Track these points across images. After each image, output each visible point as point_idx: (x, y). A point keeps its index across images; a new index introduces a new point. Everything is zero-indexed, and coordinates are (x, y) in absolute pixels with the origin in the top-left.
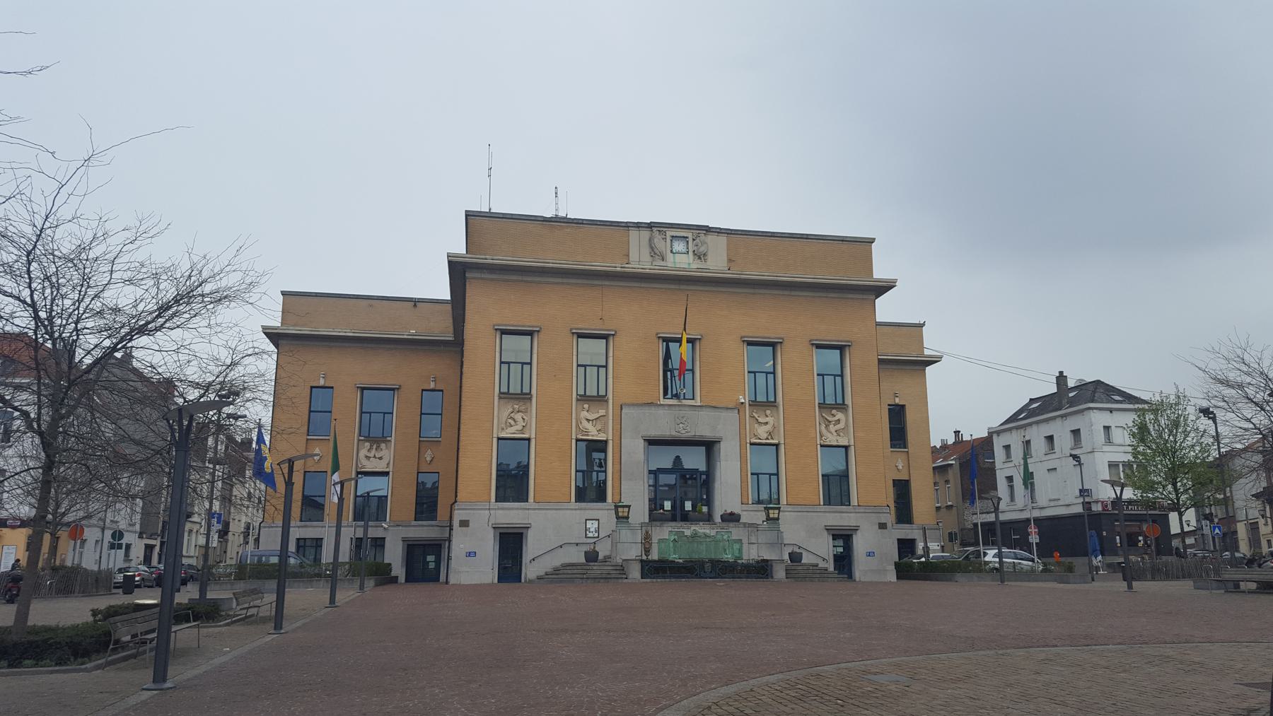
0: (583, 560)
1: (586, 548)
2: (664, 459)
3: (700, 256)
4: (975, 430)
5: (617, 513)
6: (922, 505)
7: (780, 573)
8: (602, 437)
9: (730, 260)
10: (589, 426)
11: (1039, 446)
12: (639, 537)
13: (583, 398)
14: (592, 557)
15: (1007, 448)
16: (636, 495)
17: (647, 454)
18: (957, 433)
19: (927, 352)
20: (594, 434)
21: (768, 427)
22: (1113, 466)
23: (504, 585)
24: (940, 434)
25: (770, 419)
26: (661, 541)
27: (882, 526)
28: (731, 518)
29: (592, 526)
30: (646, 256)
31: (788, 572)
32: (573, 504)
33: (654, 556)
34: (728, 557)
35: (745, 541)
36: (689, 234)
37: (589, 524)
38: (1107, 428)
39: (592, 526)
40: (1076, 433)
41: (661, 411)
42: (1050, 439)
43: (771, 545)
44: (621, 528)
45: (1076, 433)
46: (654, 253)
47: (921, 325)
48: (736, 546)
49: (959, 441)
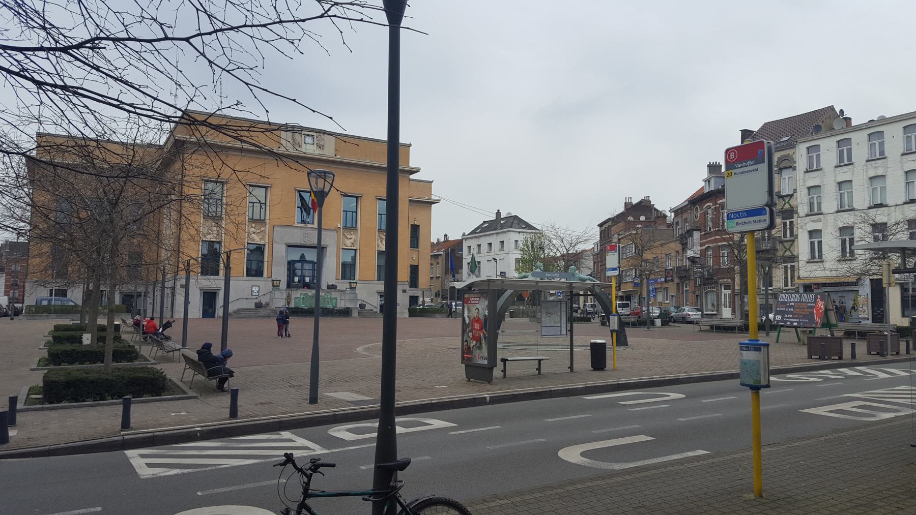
0: (253, 307)
1: (257, 301)
2: (295, 255)
3: (320, 147)
4: (454, 236)
5: (273, 284)
6: (423, 278)
7: (355, 314)
8: (262, 242)
9: (336, 150)
11: (484, 247)
12: (284, 296)
13: (252, 220)
14: (259, 305)
16: (280, 273)
17: (287, 252)
18: (446, 236)
19: (433, 197)
20: (257, 239)
21: (352, 241)
22: (517, 261)
24: (436, 235)
25: (353, 237)
28: (332, 287)
29: (256, 289)
31: (359, 313)
32: (245, 278)
33: (292, 305)
34: (330, 306)
36: (315, 134)
38: (516, 241)
39: (256, 289)
40: (502, 242)
41: (296, 230)
42: (490, 244)
43: (351, 300)
45: (502, 242)
46: (295, 144)
47: (431, 182)
49: (446, 240)
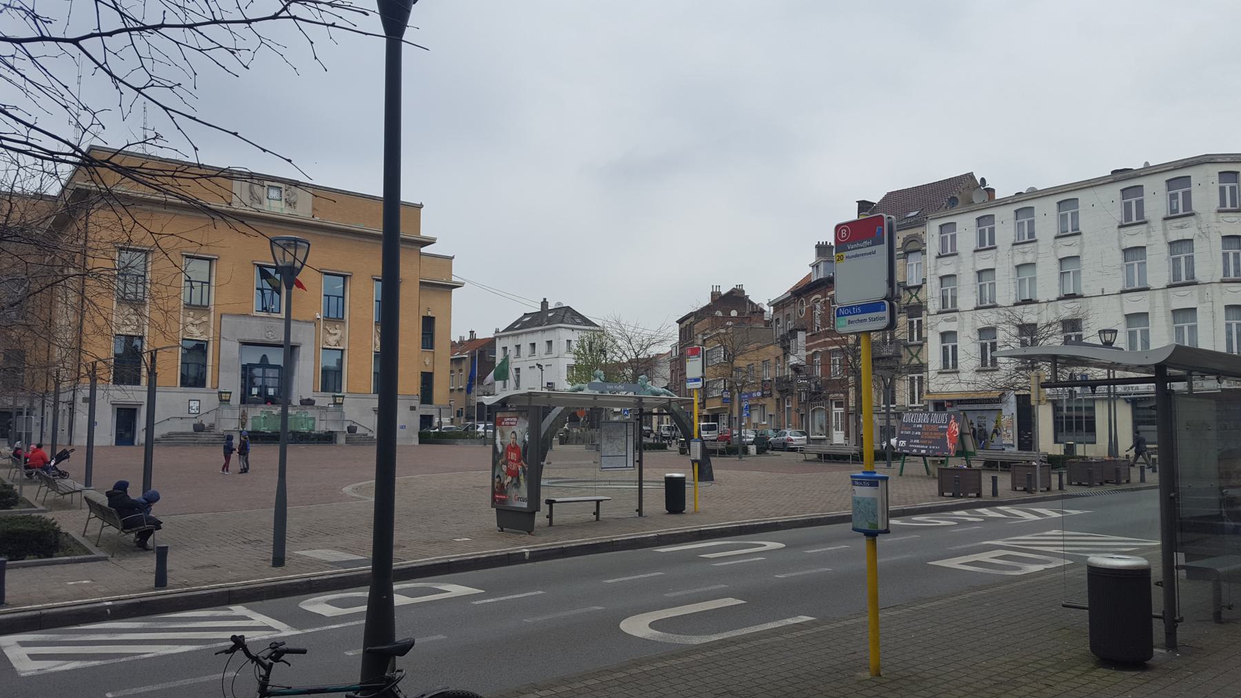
0: (191, 429)
1: (196, 421)
2: (254, 357)
3: (291, 204)
4: (484, 333)
7: (341, 440)
9: (314, 209)
10: (193, 329)
12: (237, 414)
14: (199, 428)
15: (505, 348)
16: (232, 383)
17: (240, 351)
18: (472, 332)
19: (454, 279)
20: (197, 333)
21: (337, 337)
22: (570, 368)
23: (119, 448)
24: (459, 330)
25: (338, 332)
26: (254, 418)
27: (413, 408)
28: (308, 403)
29: (194, 405)
30: (246, 199)
32: (179, 388)
33: (249, 428)
34: (304, 429)
35: (317, 419)
36: (283, 186)
37: (192, 404)
38: (569, 341)
39: (194, 405)
40: (550, 343)
41: (254, 321)
42: (533, 345)
43: (336, 421)
44: (214, 405)
45: (550, 343)
48: (311, 422)
49: (473, 339)
